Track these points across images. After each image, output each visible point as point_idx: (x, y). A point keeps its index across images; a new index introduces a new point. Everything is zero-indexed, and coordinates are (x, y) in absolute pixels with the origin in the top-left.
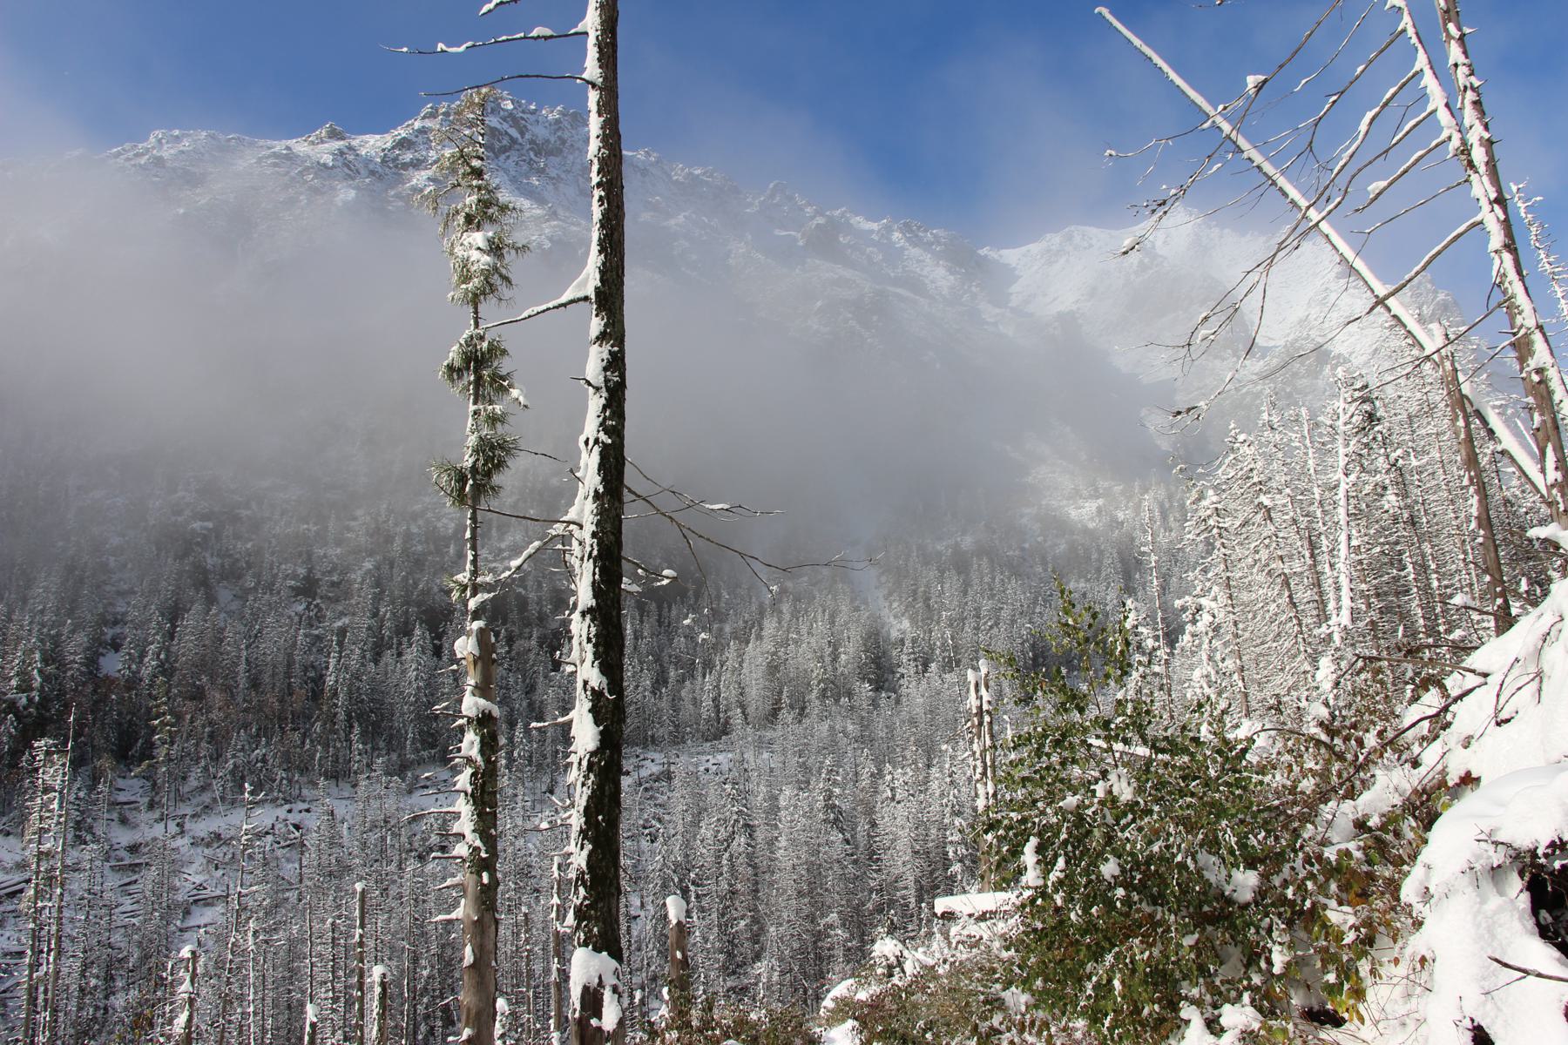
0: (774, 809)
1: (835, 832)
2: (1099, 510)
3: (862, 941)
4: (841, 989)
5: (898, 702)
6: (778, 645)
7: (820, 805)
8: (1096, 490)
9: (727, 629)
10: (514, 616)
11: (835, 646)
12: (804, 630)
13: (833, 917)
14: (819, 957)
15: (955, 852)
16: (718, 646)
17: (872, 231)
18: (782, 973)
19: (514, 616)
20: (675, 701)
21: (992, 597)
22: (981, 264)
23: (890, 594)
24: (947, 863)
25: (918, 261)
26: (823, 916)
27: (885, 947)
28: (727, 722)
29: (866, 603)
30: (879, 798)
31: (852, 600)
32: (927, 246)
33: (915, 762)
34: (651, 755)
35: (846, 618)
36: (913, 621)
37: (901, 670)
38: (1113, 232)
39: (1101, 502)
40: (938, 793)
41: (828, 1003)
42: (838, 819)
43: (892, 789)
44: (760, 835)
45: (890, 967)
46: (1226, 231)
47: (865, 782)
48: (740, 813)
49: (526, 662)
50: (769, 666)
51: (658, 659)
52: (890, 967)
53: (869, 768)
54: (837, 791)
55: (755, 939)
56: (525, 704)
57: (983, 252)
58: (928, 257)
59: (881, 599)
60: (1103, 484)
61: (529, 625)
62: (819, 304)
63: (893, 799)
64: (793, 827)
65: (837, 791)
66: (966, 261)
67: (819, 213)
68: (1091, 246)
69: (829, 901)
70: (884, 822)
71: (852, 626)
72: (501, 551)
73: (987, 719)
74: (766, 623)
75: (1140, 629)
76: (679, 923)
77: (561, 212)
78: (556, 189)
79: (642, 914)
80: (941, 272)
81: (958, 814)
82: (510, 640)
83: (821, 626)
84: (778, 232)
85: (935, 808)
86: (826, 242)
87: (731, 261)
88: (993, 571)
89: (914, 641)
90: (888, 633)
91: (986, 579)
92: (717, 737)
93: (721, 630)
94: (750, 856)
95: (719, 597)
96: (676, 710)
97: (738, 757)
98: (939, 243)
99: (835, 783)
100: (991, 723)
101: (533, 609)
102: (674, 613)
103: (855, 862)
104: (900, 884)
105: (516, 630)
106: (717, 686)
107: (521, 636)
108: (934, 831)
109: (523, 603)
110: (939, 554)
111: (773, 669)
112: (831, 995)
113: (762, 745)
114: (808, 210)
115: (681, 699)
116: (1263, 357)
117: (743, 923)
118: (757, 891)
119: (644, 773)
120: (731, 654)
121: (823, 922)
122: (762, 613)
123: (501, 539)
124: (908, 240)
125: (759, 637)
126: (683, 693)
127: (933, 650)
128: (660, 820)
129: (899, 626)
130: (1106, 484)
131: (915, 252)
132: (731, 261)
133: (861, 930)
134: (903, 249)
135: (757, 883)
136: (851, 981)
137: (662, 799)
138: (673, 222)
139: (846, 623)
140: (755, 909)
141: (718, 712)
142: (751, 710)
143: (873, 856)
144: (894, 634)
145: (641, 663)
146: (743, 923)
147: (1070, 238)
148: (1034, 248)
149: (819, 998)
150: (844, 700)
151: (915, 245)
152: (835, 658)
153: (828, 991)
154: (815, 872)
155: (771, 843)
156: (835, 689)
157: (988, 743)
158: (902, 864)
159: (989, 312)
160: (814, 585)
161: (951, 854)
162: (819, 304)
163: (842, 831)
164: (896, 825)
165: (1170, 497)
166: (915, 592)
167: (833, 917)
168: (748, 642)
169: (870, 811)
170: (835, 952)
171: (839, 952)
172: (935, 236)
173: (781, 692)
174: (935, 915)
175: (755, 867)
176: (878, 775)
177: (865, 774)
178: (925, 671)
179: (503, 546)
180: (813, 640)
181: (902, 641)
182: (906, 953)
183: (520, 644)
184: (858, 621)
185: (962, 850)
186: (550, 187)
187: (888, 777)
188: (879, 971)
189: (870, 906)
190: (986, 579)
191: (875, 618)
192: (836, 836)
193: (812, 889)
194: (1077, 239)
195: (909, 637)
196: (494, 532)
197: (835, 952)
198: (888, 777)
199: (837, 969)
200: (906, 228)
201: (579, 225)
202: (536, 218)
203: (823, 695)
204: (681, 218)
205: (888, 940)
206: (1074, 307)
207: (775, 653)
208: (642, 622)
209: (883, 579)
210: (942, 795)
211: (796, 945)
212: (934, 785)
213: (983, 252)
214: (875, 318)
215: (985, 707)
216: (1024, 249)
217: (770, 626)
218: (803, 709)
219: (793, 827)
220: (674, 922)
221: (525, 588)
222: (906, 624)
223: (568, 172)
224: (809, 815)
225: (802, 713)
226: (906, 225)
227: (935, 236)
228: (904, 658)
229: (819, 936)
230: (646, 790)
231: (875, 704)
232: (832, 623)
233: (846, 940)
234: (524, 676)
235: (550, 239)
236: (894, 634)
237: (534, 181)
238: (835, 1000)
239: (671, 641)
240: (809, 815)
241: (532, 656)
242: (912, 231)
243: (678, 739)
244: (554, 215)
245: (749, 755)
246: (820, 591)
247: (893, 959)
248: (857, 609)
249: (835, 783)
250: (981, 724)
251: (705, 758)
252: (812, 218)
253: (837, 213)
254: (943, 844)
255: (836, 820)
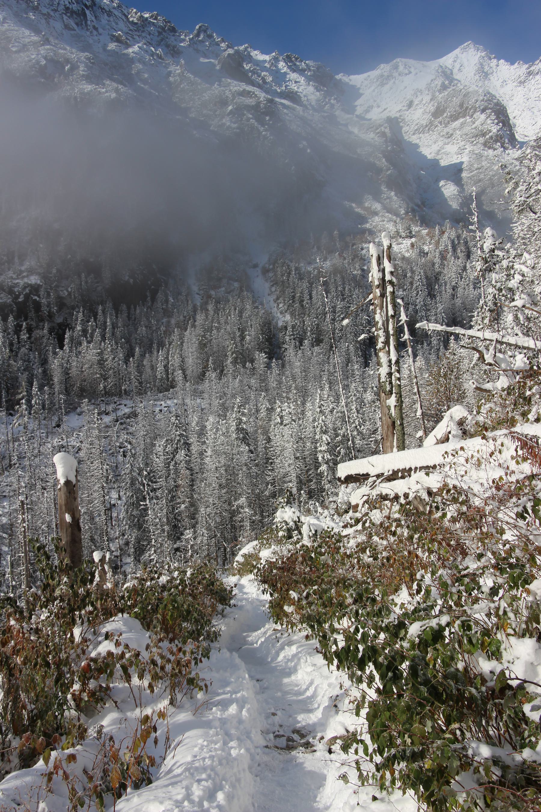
0: (202, 433)
1: (243, 446)
2: (412, 245)
3: (262, 516)
4: (248, 549)
5: (283, 366)
6: (206, 331)
7: (233, 428)
8: (411, 232)
9: (173, 321)
10: (32, 314)
11: (242, 331)
12: (222, 321)
13: (242, 500)
14: (233, 527)
15: (323, 458)
16: (168, 333)
17: (265, 61)
18: (210, 538)
19: (32, 314)
20: (140, 368)
21: (343, 299)
22: (338, 85)
23: (278, 299)
24: (317, 465)
25: (296, 82)
26: (235, 500)
27: (286, 514)
28: (173, 380)
29: (262, 304)
30: (272, 423)
31: (254, 302)
32: (301, 72)
33: (296, 401)
34: (124, 402)
35: (249, 313)
36: (292, 314)
37: (285, 346)
38: (425, 63)
39: (413, 240)
40: (311, 419)
41: (239, 558)
42: (245, 437)
43: (281, 417)
44: (194, 449)
45: (289, 530)
46: (502, 61)
47: (263, 414)
48: (181, 435)
49: (41, 344)
50: (200, 343)
51: (128, 341)
52: (289, 530)
53: (264, 406)
54: (244, 419)
55: (193, 516)
56: (40, 370)
57: (339, 77)
58: (302, 80)
59: (272, 302)
60: (415, 229)
61: (42, 320)
62: (230, 108)
63: (281, 423)
64: (216, 441)
65: (244, 419)
66: (321, 79)
67: (228, 47)
68: (410, 73)
69: (239, 491)
70: (276, 441)
71: (254, 318)
72: (21, 272)
73: (389, 289)
74: (198, 317)
75: (497, 252)
76: (68, 483)
77: (51, 39)
78: (48, 23)
79: (119, 502)
80: (311, 89)
81: (325, 432)
82: (30, 330)
83: (233, 318)
84: (202, 60)
85: (310, 429)
86: (236, 67)
87: (171, 79)
88: (344, 284)
89: (293, 327)
90: (277, 323)
91: (340, 289)
92: (167, 390)
93: (169, 322)
94: (188, 462)
95: (167, 301)
96: (140, 372)
97: (180, 402)
98: (310, 70)
99: (243, 414)
100: (393, 293)
101: (45, 310)
102: (138, 311)
103: (257, 465)
104: (287, 479)
105: (34, 324)
106: (167, 358)
107: (37, 327)
108: (308, 444)
109: (37, 306)
110: (309, 273)
111: (202, 346)
112: (241, 552)
113: (197, 394)
114: (223, 45)
115: (143, 365)
116: (521, 148)
117: (183, 506)
118: (192, 485)
119: (120, 413)
120: (175, 337)
121: (236, 503)
122: (195, 311)
123: (21, 264)
124: (289, 67)
125: (194, 326)
126: (145, 363)
127: (305, 333)
128: (130, 443)
129: (284, 319)
130: (417, 229)
131: (293, 76)
132: (171, 79)
133: (264, 508)
134: (286, 74)
135: (193, 480)
136: (255, 543)
137: (131, 429)
138: (130, 50)
139: (250, 316)
140: (192, 497)
141: (167, 374)
142: (189, 372)
143: (268, 460)
144: (280, 324)
145: (117, 343)
146: (183, 506)
147: (396, 67)
148: (374, 74)
149: (234, 555)
150: (248, 365)
151: (294, 71)
152: (243, 338)
153: (240, 549)
154: (231, 471)
155: (201, 454)
156: (244, 358)
157: (391, 312)
158: (287, 465)
159: (341, 116)
160: (229, 293)
161: (320, 459)
162: (230, 108)
163: (248, 445)
164: (284, 441)
165: (458, 237)
166: (294, 297)
167: (242, 500)
168: (186, 330)
169: (266, 432)
170: (245, 524)
171: (247, 524)
172: (307, 65)
173: (208, 361)
174: (335, 478)
175: (191, 469)
176: (271, 410)
177: (263, 414)
178: (301, 345)
179: (23, 268)
180: (228, 327)
181: (286, 328)
182: (303, 519)
183: (37, 333)
184: (257, 314)
185: (327, 456)
186: (43, 21)
187: (279, 410)
188: (281, 534)
189: (267, 493)
190: (340, 289)
191: (268, 313)
192: (244, 448)
193: (229, 486)
194: (401, 68)
195: (290, 324)
196: (16, 260)
197: (245, 524)
198: (279, 410)
199: (246, 534)
200: (288, 59)
201: (66, 49)
202: (34, 43)
203: (235, 362)
204: (136, 48)
205: (287, 509)
206: (398, 115)
207: (204, 336)
208: (117, 317)
209: (273, 289)
210: (314, 420)
211: (218, 520)
212: (309, 414)
213: (339, 77)
214: (267, 118)
215: (388, 277)
216: (365, 75)
217: (200, 318)
218: (222, 371)
219: (216, 441)
220: (62, 481)
221: (39, 297)
222: (288, 317)
223: (56, 11)
224: (226, 434)
225: (221, 374)
226: (288, 57)
227: (307, 65)
228: (287, 338)
229: (233, 513)
230: (121, 424)
231: (268, 366)
232: (241, 317)
233: (252, 515)
234: (40, 354)
235: (45, 58)
236: (280, 324)
237: (31, 16)
238: (244, 556)
239: (136, 330)
240: (226, 434)
241: (45, 340)
242: (291, 61)
243: (142, 392)
244: (47, 41)
245: (188, 401)
246: (233, 297)
247: (291, 524)
248: (257, 307)
249: (243, 414)
250: (383, 295)
251: (159, 403)
252: (225, 50)
253: (242, 48)
254: (315, 452)
255: (244, 438)
